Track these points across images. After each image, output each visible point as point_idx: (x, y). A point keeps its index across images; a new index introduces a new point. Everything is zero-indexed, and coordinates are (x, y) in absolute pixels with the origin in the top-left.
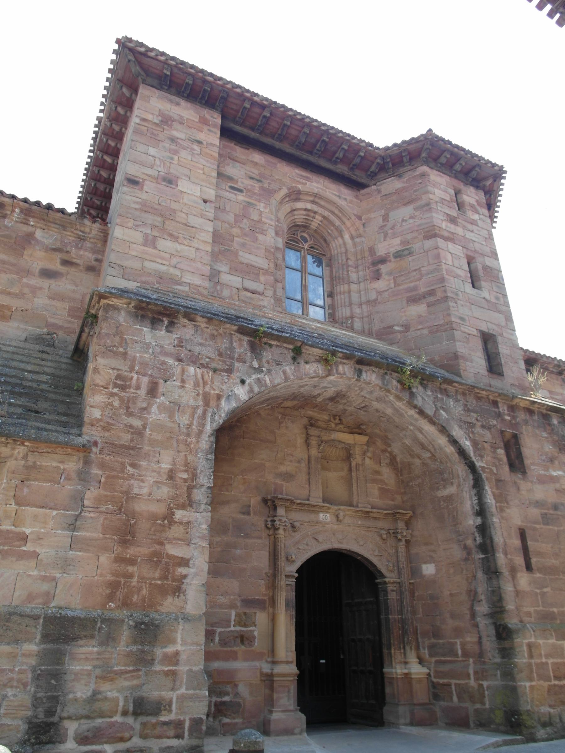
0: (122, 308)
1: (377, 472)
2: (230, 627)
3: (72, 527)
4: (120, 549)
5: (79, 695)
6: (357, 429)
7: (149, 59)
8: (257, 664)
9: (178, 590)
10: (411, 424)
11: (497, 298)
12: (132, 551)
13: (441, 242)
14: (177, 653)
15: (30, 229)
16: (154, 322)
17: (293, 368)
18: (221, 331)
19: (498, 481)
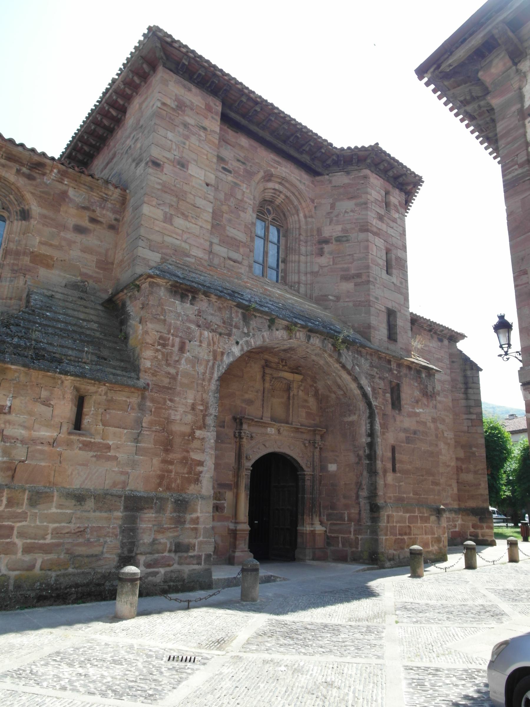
0: (162, 285)
1: (306, 401)
3: (136, 440)
5: (146, 541)
6: (296, 370)
7: (172, 49)
8: (226, 523)
9: (197, 481)
10: (335, 372)
11: (401, 283)
12: (171, 456)
13: (370, 236)
14: (198, 518)
15: (65, 188)
16: (183, 297)
18: (225, 305)
19: (384, 415)
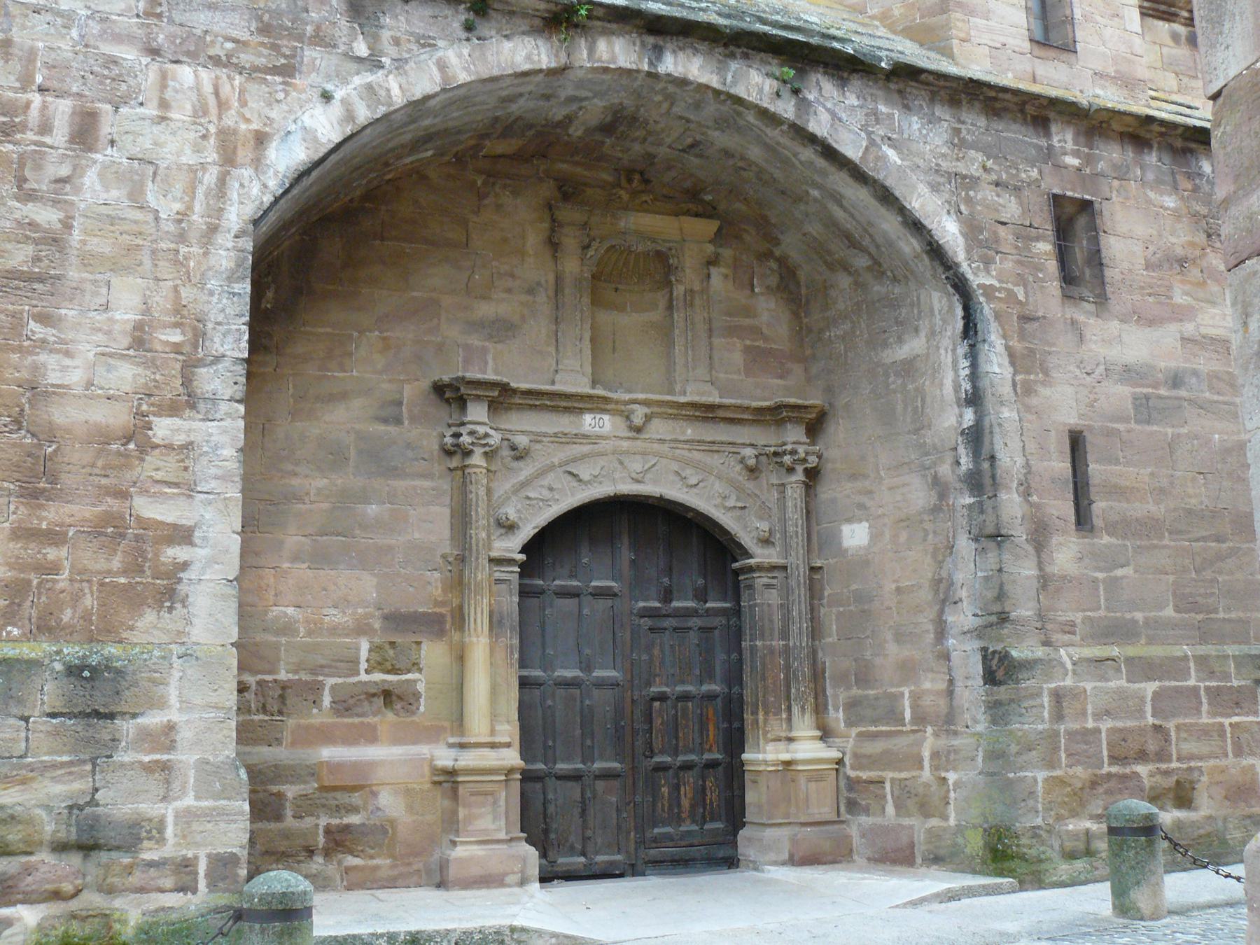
2: (358, 674)
4: (22, 510)
6: (691, 200)
8: (424, 750)
9: (168, 593)
12: (51, 514)
14: (171, 727)
17: (466, 52)
